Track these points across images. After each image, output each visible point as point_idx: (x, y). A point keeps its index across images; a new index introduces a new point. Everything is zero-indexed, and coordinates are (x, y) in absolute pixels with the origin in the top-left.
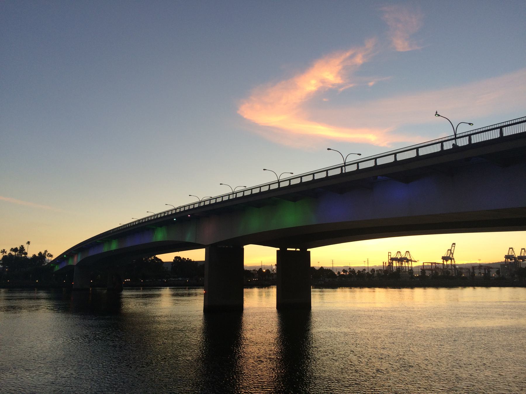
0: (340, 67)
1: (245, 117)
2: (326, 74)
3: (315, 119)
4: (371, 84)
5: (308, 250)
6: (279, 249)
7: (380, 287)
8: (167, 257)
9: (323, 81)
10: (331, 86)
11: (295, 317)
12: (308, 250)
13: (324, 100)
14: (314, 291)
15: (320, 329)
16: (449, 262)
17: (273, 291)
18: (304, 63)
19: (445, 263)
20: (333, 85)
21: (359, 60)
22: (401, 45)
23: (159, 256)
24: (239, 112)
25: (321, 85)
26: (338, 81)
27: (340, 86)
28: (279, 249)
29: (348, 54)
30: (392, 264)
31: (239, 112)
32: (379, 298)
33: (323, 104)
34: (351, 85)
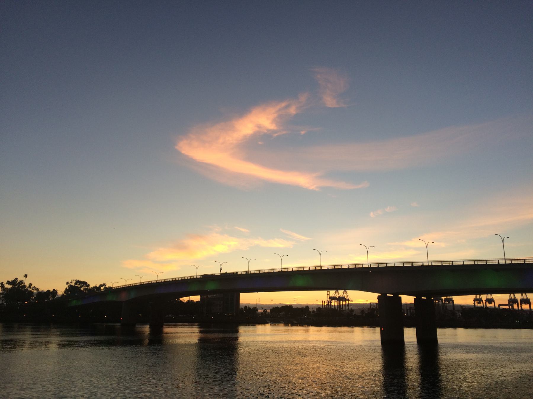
0: (276, 115)
1: (183, 152)
2: (261, 120)
3: (250, 159)
4: (303, 133)
5: (400, 296)
6: (415, 297)
7: (328, 325)
8: (185, 299)
9: (259, 126)
10: (265, 131)
11: (429, 347)
12: (400, 296)
13: (260, 143)
14: (245, 331)
15: (446, 356)
16: (492, 305)
17: (378, 330)
18: (243, 108)
19: (476, 304)
20: (269, 130)
21: (293, 111)
22: (330, 102)
23: (182, 299)
24: (177, 147)
25: (257, 129)
26: (272, 127)
27: (274, 132)
28: (415, 297)
29: (283, 105)
30: (331, 303)
31: (177, 147)
32: (318, 335)
33: (257, 147)
34: (284, 132)
